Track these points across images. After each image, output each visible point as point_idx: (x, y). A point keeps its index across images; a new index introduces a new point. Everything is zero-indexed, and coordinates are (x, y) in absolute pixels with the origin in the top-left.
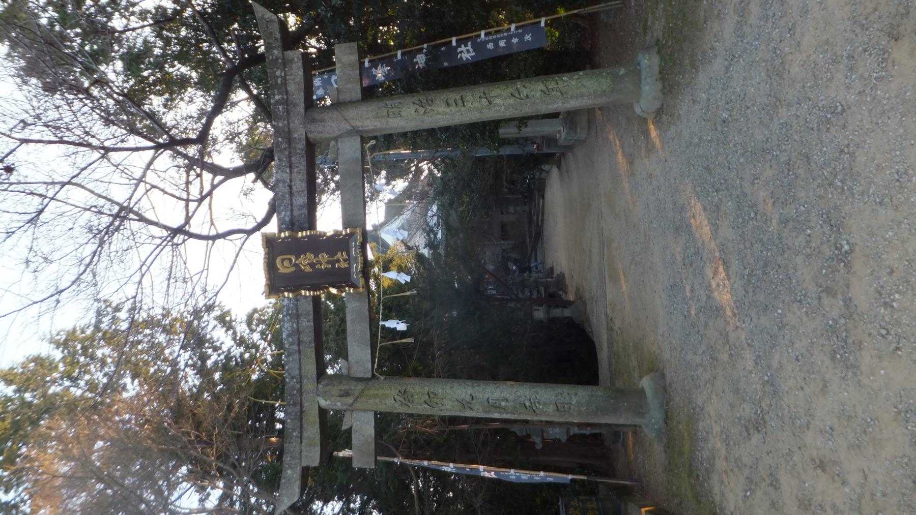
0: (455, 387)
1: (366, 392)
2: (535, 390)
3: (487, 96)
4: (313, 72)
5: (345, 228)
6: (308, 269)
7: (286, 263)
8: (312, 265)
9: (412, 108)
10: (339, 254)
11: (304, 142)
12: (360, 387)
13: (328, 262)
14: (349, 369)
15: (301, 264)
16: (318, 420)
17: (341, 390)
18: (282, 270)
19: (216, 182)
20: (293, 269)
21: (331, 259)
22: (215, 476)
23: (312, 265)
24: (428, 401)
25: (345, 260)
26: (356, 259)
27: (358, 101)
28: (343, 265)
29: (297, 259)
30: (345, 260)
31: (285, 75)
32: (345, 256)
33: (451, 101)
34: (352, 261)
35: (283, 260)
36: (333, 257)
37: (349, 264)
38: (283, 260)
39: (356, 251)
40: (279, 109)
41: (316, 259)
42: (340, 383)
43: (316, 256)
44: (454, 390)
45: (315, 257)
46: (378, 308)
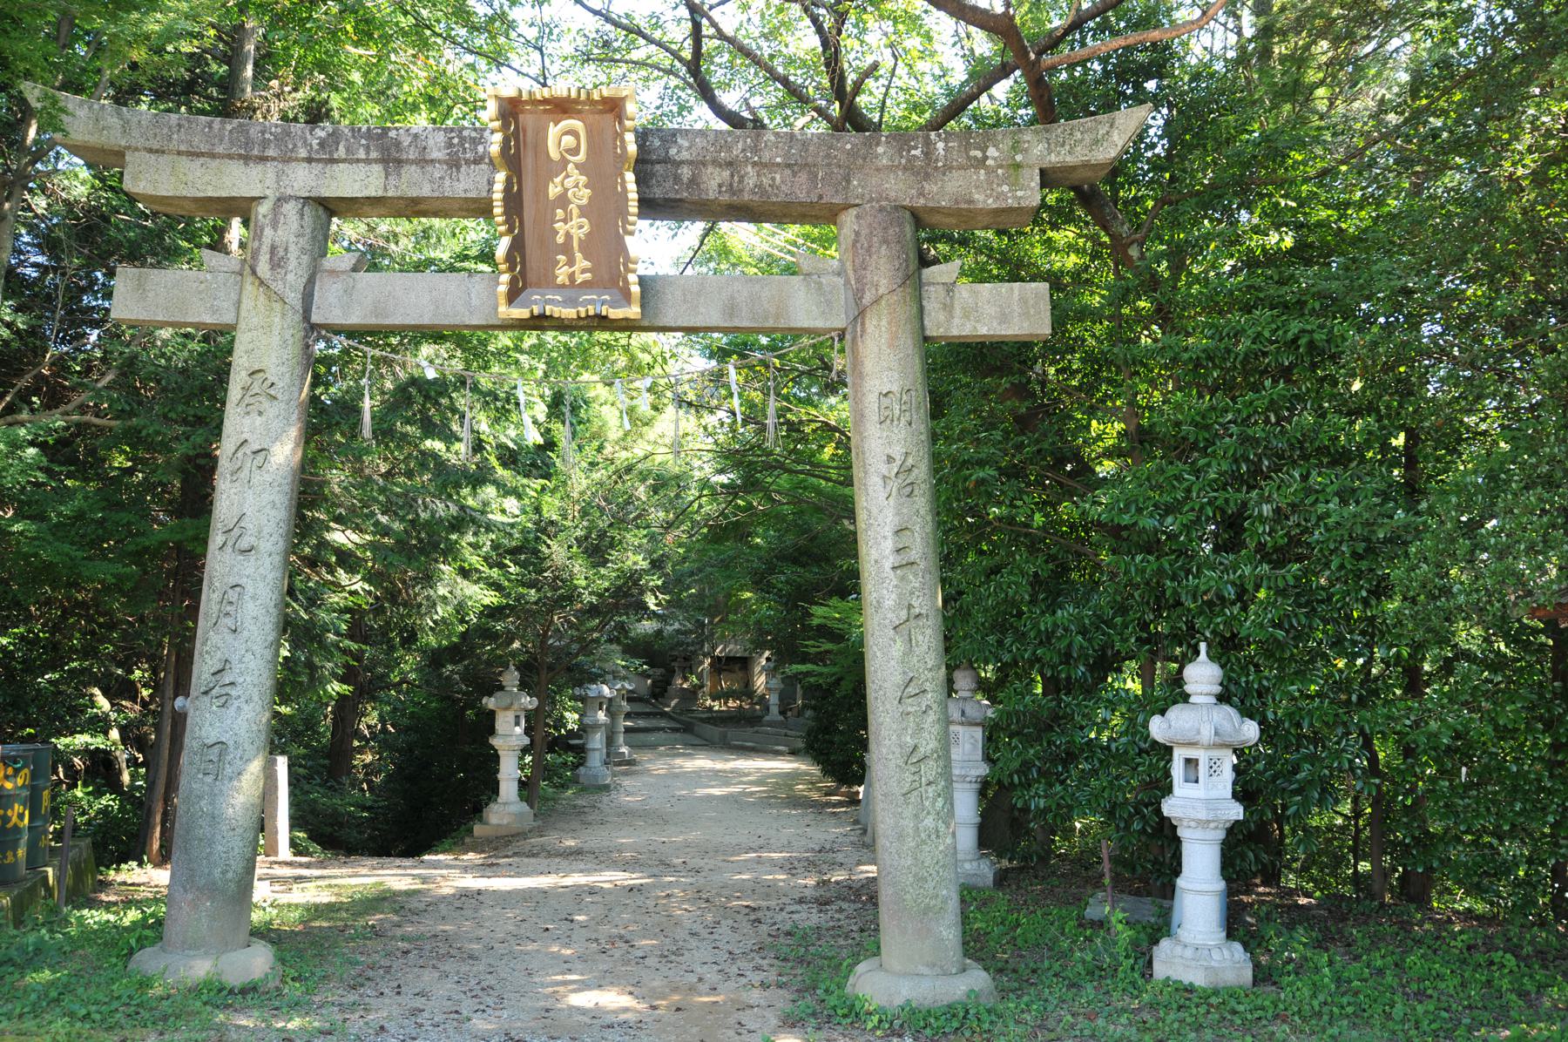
0: (273, 513)
1: (277, 306)
2: (256, 698)
3: (913, 623)
4: (588, 276)
5: (642, 281)
6: (554, 191)
7: (569, 141)
8: (563, 201)
9: (897, 451)
10: (587, 264)
11: (837, 200)
12: (294, 298)
13: (568, 236)
14: (333, 272)
15: (567, 176)
16: (224, 195)
17: (286, 250)
18: (553, 131)
19: (712, 31)
20: (554, 154)
21: (575, 244)
22: (1083, 870)
23: (563, 201)
24: (247, 449)
25: (572, 276)
26: (571, 302)
27: (923, 328)
28: (562, 275)
29: (577, 166)
30: (572, 276)
31: (986, 168)
32: (580, 279)
33: (906, 540)
34: (571, 293)
35: (573, 133)
36: (580, 250)
37: (563, 286)
38: (573, 133)
39: (591, 302)
40: (916, 148)
41: (576, 212)
42: (303, 251)
43: (583, 212)
44: (267, 510)
45: (579, 207)
46: (419, 876)
